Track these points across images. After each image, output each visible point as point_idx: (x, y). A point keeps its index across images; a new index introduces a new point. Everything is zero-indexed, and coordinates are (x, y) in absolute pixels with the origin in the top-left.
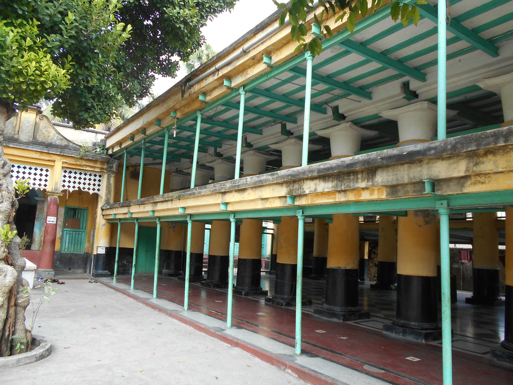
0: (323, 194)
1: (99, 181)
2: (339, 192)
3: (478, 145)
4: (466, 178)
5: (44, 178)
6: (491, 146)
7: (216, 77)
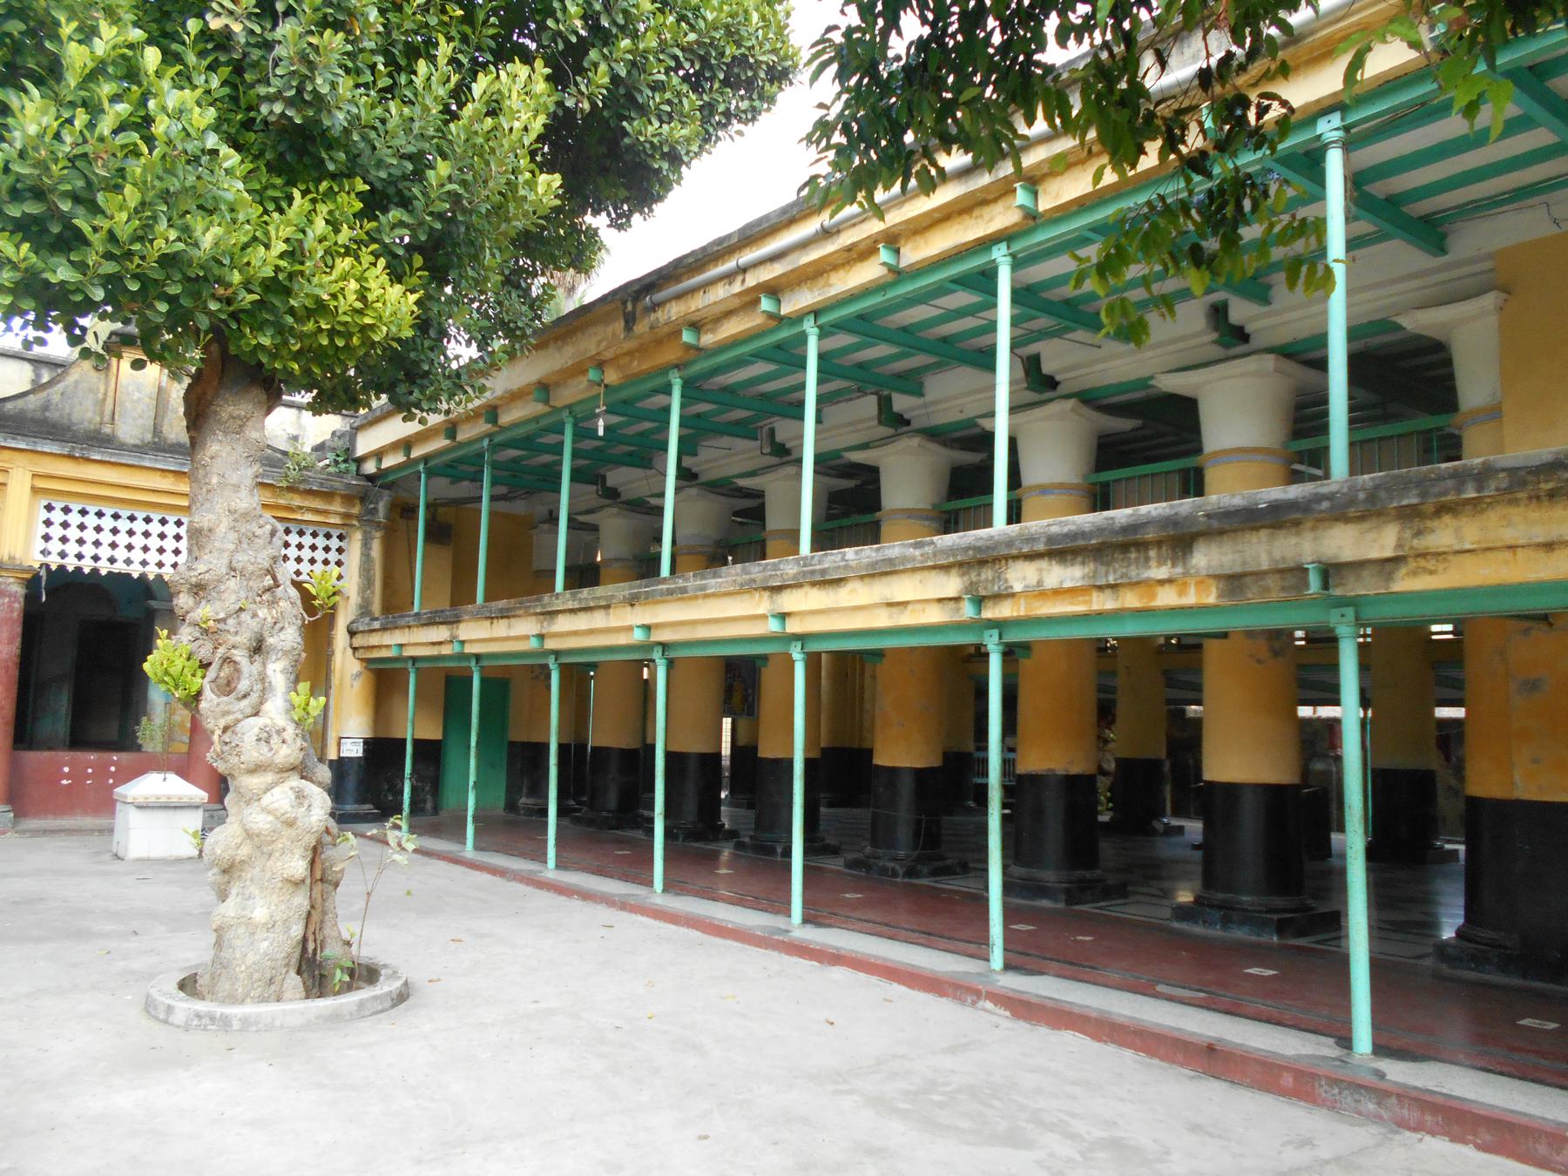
0: (1058, 593)
1: (340, 550)
2: (1100, 588)
3: (1424, 495)
4: (1396, 561)
5: (56, 531)
6: (1449, 497)
7: (737, 288)
